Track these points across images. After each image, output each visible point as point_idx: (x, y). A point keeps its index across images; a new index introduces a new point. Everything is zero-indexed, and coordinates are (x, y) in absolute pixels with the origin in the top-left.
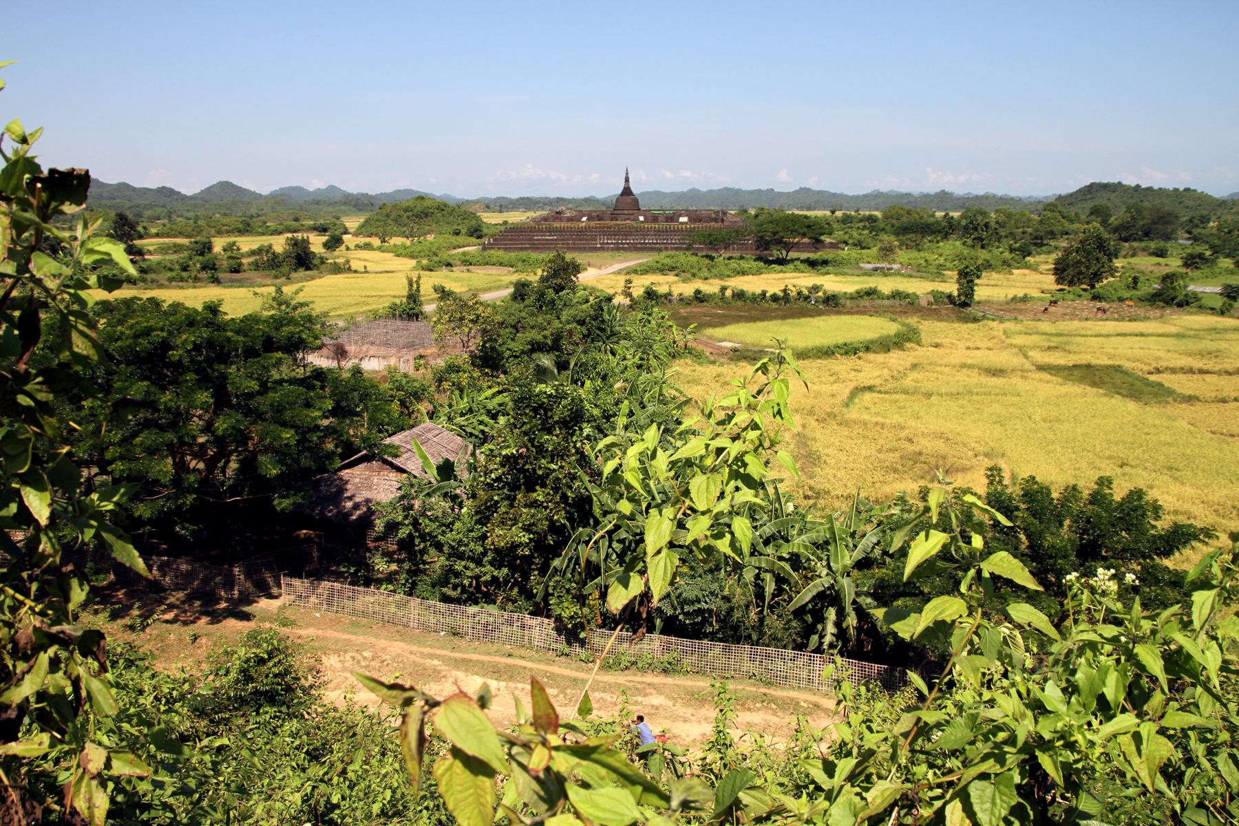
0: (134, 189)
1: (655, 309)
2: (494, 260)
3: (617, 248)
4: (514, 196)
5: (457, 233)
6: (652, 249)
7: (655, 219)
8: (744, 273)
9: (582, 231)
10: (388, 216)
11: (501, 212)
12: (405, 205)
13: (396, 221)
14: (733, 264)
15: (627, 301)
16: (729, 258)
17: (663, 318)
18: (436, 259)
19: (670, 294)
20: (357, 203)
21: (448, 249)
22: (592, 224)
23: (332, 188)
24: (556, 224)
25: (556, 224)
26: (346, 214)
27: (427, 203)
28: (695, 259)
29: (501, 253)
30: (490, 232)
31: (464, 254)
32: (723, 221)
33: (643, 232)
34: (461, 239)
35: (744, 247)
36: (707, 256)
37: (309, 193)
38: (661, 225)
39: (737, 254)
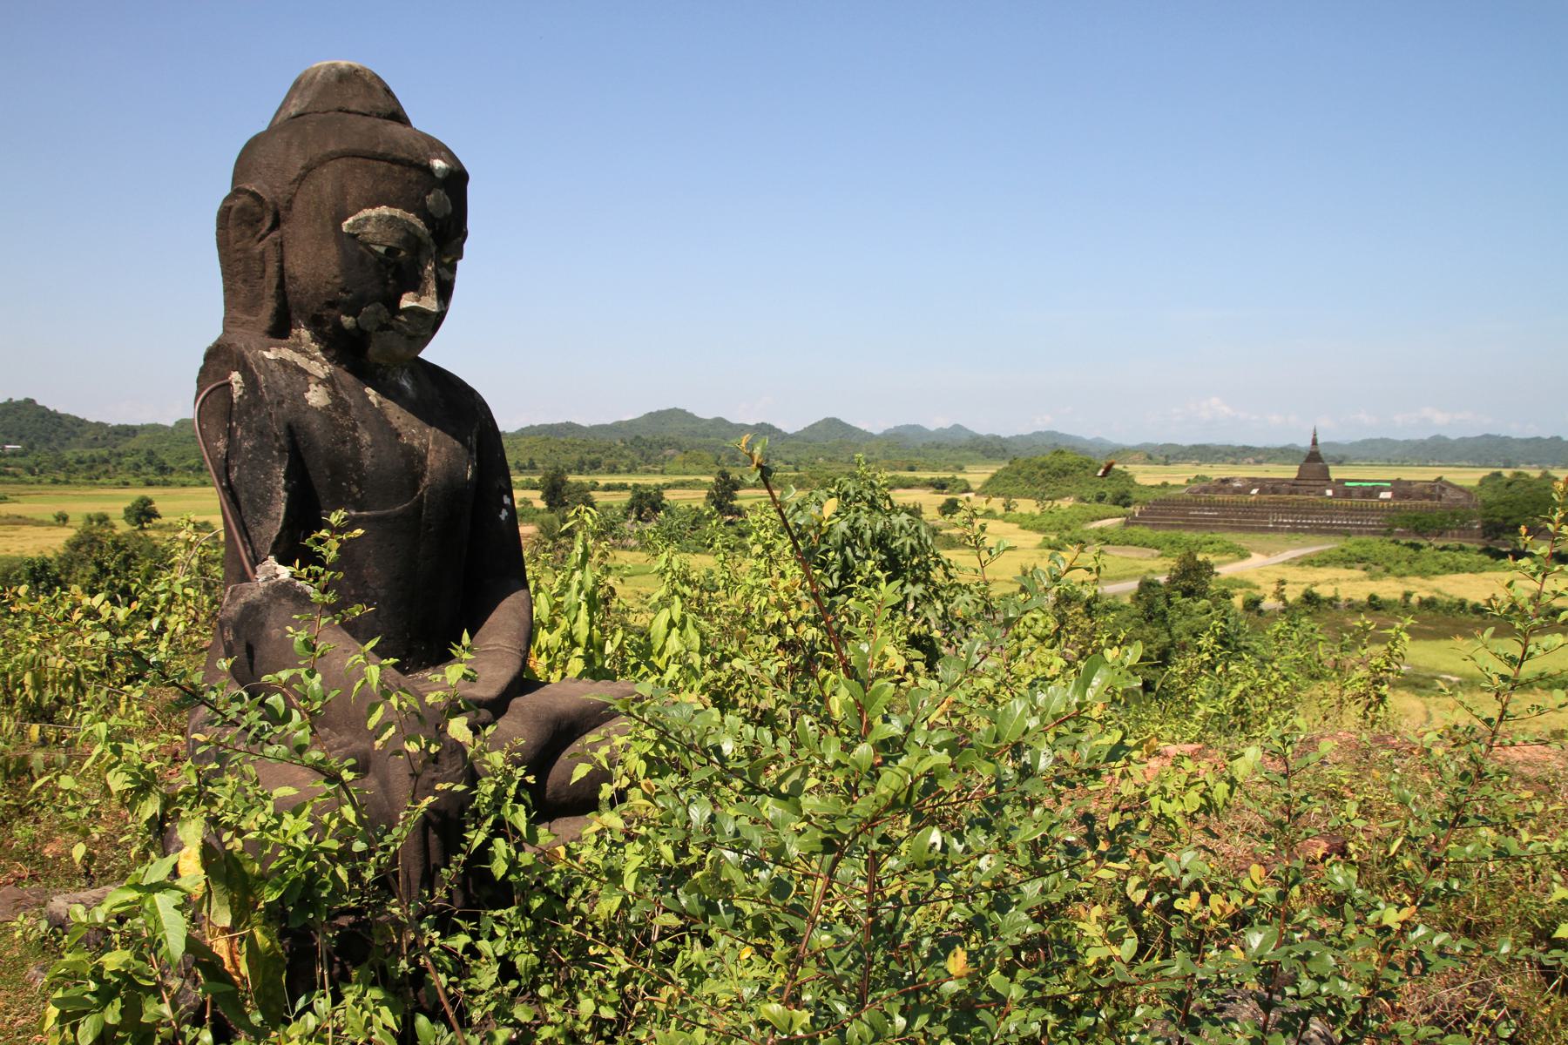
0: (731, 425)
1: (1305, 620)
2: (1137, 539)
3: (1295, 530)
4: (1187, 441)
5: (1100, 499)
6: (1340, 533)
7: (1348, 493)
8: (1458, 569)
9: (1250, 507)
10: (1019, 473)
11: (1166, 464)
12: (1040, 459)
13: (1028, 479)
14: (1445, 557)
15: (1280, 605)
16: (1444, 548)
17: (1312, 630)
18: (1067, 534)
19: (1336, 598)
20: (987, 448)
21: (1085, 521)
22: (1265, 497)
23: (958, 428)
24: (1219, 497)
25: (1219, 497)
26: (971, 461)
27: (1068, 458)
28: (1394, 547)
29: (1146, 531)
30: (1142, 497)
31: (1101, 530)
32: (1440, 498)
33: (1329, 510)
34: (1102, 508)
35: (1465, 532)
36: (1411, 545)
37: (929, 434)
38: (1356, 502)
39: (1453, 543)
